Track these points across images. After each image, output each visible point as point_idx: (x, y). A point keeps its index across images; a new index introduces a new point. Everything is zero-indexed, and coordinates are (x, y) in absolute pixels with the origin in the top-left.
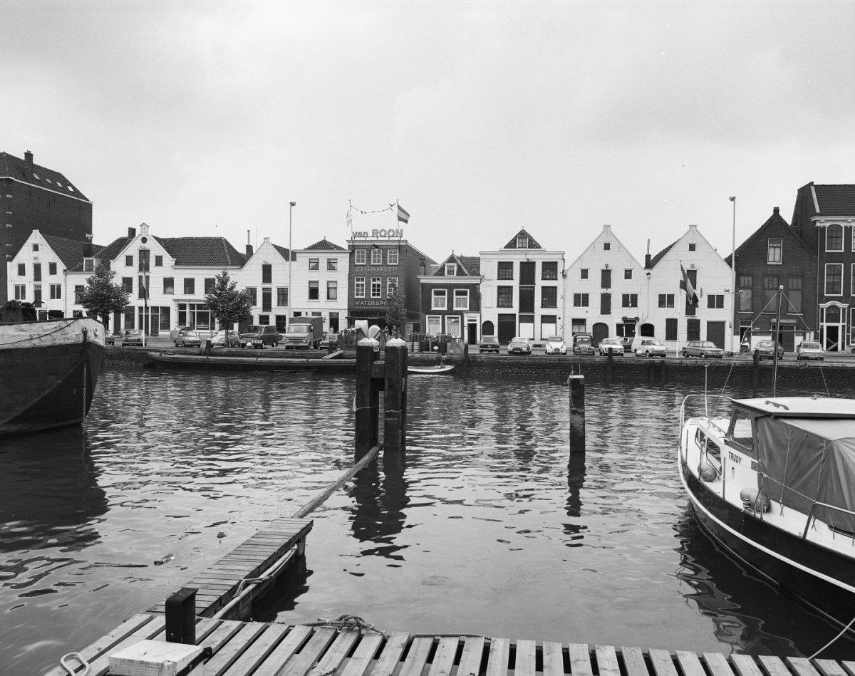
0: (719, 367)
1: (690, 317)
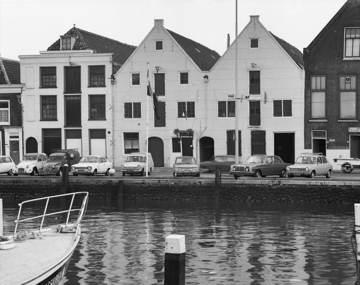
0: (183, 187)
1: (254, 128)
